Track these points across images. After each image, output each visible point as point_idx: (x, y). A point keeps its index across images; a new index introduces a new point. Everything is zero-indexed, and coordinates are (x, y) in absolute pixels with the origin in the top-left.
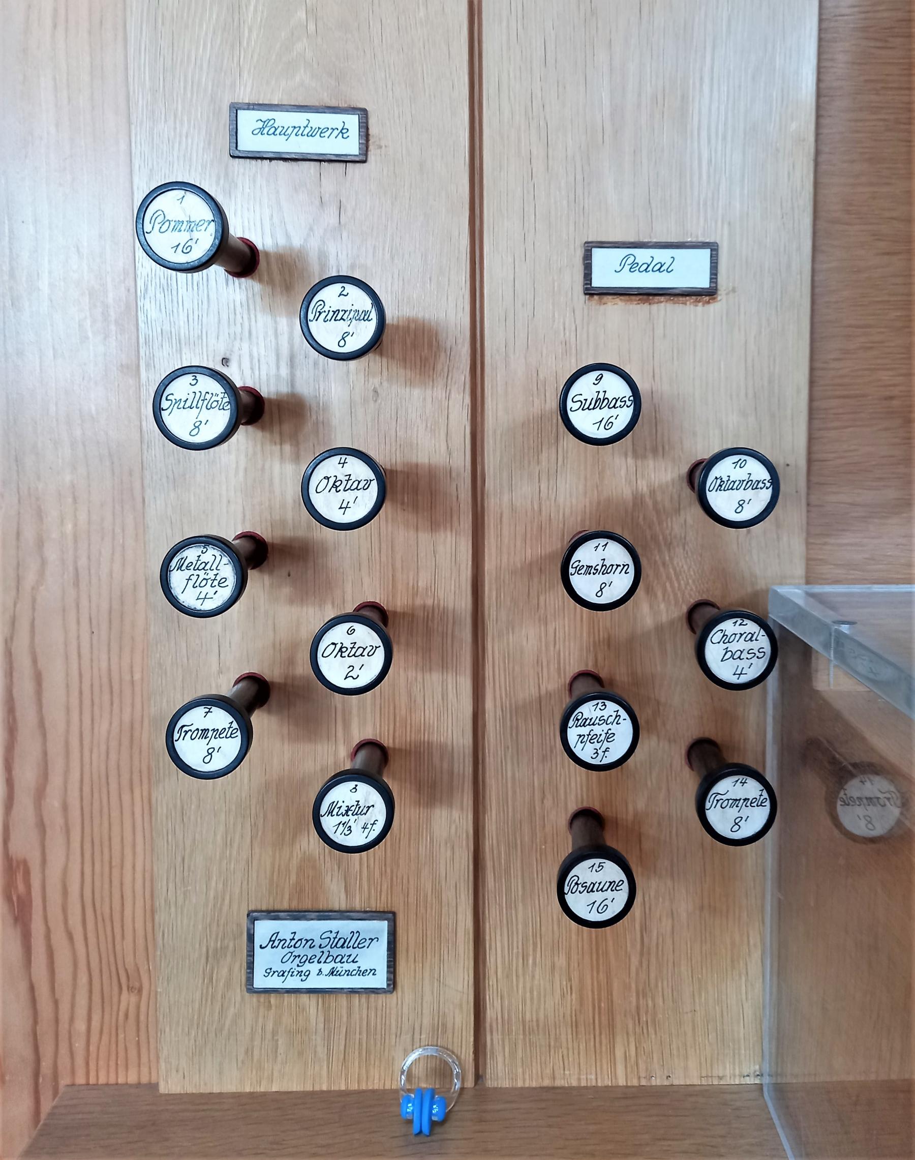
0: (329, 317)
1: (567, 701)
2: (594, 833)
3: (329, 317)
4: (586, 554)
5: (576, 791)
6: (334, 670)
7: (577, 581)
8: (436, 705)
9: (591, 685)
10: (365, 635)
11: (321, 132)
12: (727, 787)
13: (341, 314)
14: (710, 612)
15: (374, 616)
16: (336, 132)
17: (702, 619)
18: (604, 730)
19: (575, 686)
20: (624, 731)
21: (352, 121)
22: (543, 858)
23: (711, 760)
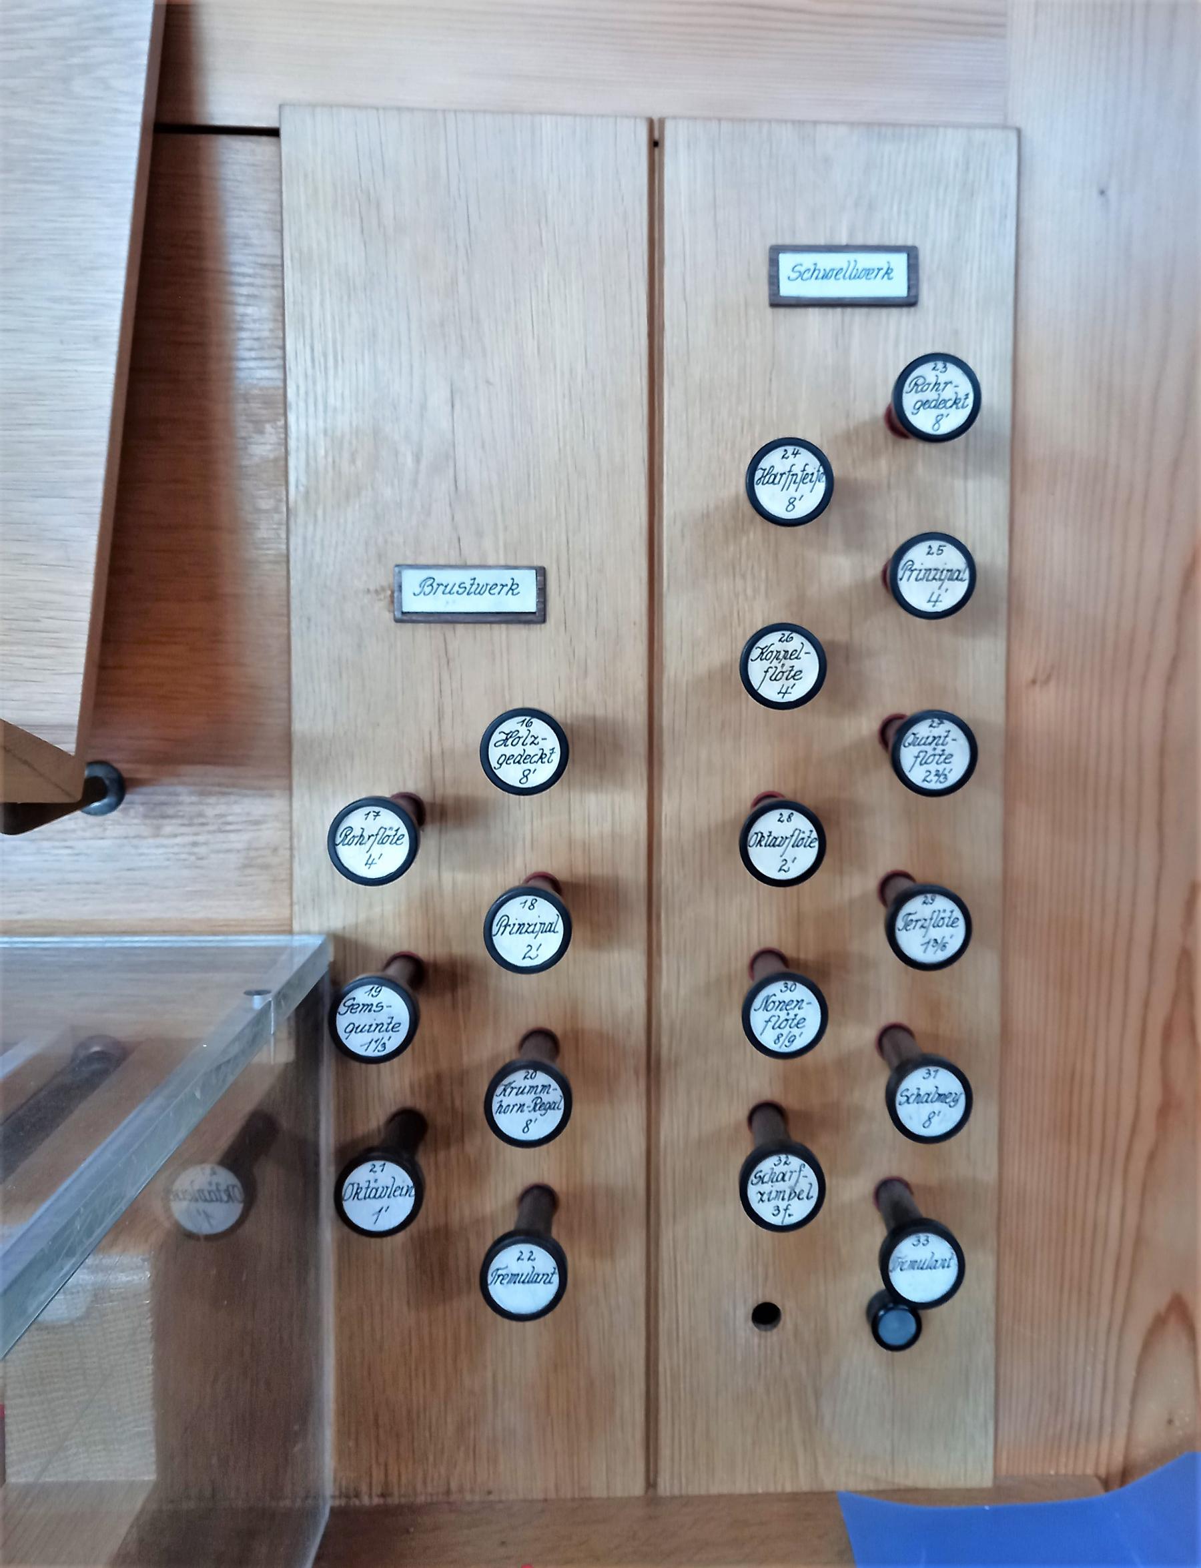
0: (921, 576)
1: (747, 985)
2: (776, 1129)
3: (921, 576)
4: (769, 823)
5: (761, 1081)
6: (511, 947)
7: (755, 854)
8: (609, 985)
9: (774, 965)
10: (546, 912)
11: (868, 272)
12: (917, 1081)
13: (933, 572)
14: (903, 885)
15: (547, 886)
16: (882, 272)
17: (896, 892)
18: (786, 1017)
19: (756, 966)
20: (812, 1014)
21: (899, 262)
22: (1083, 1441)
23: (901, 1052)
